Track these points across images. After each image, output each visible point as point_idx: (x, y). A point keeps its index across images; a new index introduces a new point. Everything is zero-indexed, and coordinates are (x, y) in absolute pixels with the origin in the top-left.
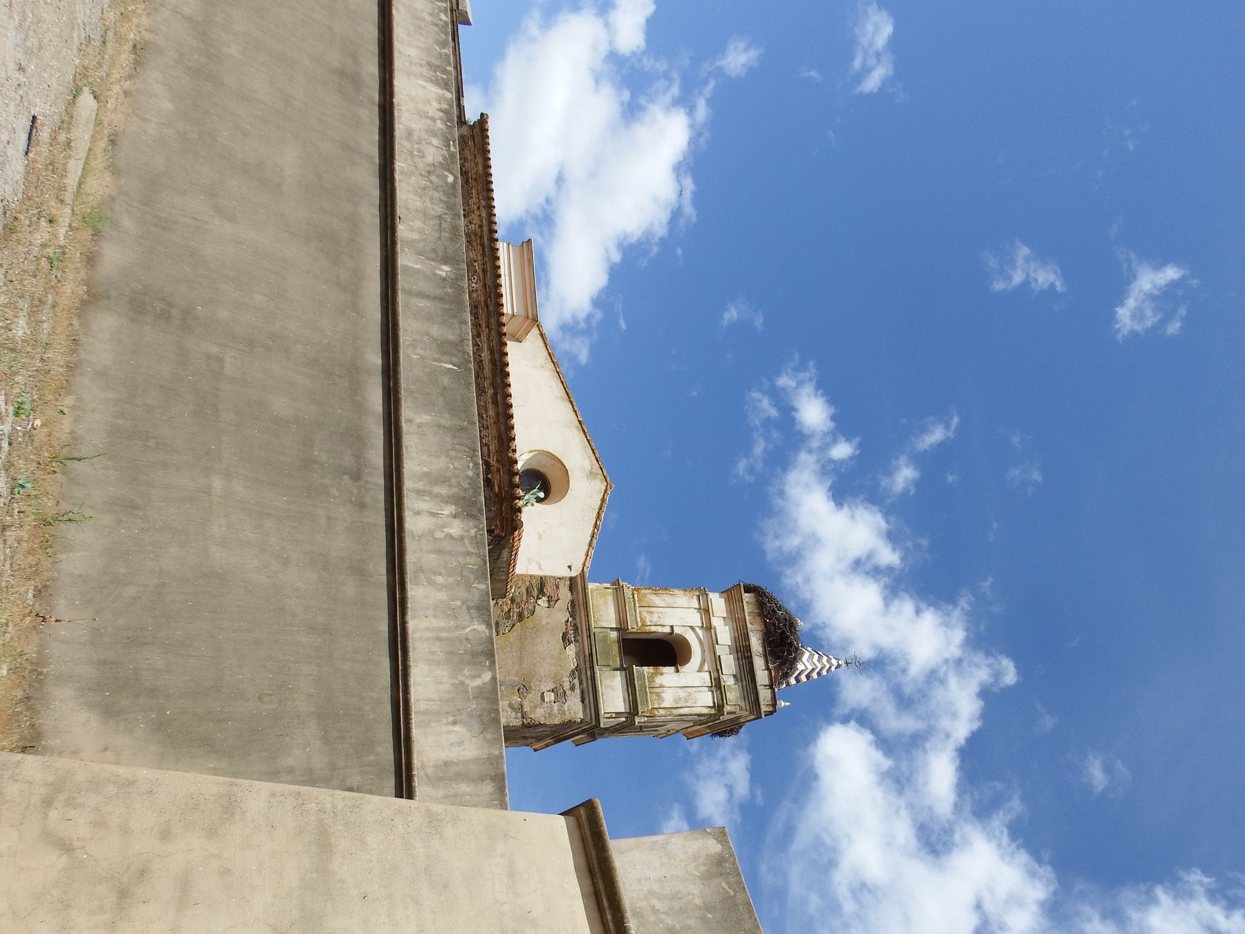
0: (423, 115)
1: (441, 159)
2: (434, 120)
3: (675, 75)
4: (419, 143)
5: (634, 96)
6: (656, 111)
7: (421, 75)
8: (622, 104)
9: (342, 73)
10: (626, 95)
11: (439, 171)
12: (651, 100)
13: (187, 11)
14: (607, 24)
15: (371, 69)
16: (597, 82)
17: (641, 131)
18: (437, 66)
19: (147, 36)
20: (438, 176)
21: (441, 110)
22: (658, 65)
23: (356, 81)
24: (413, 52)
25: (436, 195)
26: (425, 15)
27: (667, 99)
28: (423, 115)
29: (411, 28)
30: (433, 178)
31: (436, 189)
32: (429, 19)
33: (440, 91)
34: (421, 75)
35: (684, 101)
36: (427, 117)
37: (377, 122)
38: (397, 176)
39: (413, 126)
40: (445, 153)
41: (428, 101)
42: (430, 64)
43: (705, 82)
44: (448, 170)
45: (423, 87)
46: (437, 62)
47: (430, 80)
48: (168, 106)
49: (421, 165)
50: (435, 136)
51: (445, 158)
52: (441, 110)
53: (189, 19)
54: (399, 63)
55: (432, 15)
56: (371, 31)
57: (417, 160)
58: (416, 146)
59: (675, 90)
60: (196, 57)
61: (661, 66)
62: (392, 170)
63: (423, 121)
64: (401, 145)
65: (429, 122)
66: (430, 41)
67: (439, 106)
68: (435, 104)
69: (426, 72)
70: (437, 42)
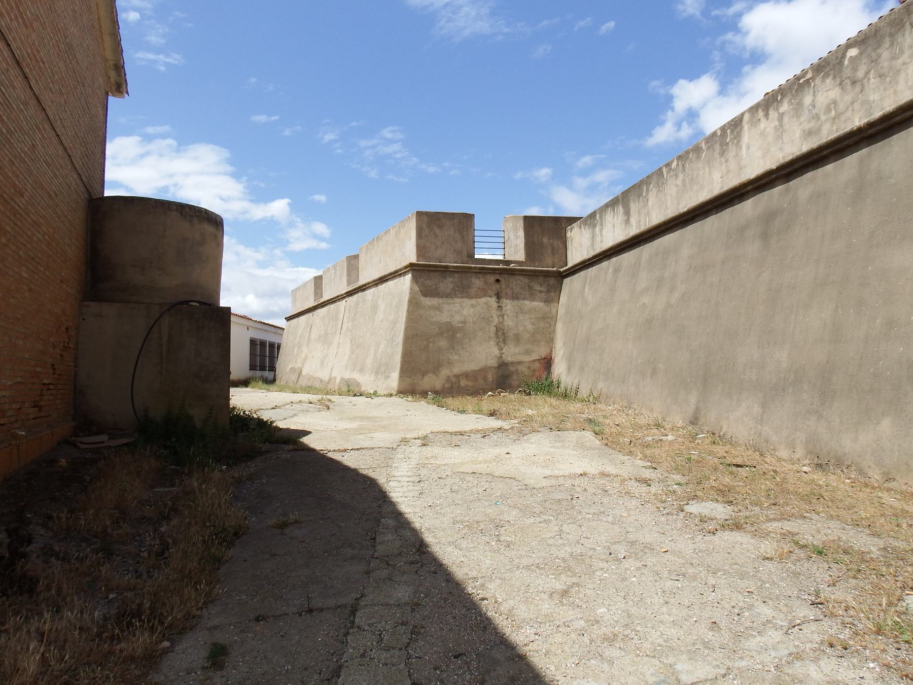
0: (780, 129)
1: (829, 81)
2: (782, 115)
3: (718, 42)
4: (817, 117)
5: (746, 63)
6: (750, 41)
7: (737, 155)
8: (754, 68)
9: (765, 236)
10: (746, 69)
11: (847, 72)
12: (744, 48)
13: (757, 409)
14: (704, 105)
15: (748, 207)
16: (745, 94)
17: (771, 44)
18: (721, 145)
19: (800, 452)
20: (855, 70)
21: (767, 115)
22: (717, 59)
23: (769, 217)
24: (716, 176)
25: (886, 55)
26: (679, 182)
27: (738, 39)
28: (780, 129)
29: (695, 188)
30: (860, 74)
31: (875, 61)
32: (681, 176)
33: (746, 127)
34: (737, 155)
35: (733, 25)
36: (781, 125)
37: (809, 175)
38: (877, 114)
39: (798, 134)
40: (818, 81)
41: (763, 134)
42: (722, 153)
43: (717, 18)
44: (841, 63)
45: (748, 147)
46: (717, 147)
47: (738, 145)
48: (886, 425)
49: (848, 98)
50: (800, 104)
51: (827, 75)
52: (767, 115)
53: (764, 405)
54: (733, 181)
55: (677, 176)
56: (712, 223)
57: (841, 106)
58: (823, 118)
59: (729, 36)
60: (805, 396)
61: (716, 55)
62: (871, 125)
63: (786, 126)
64: (828, 133)
65: (786, 119)
66: (700, 165)
67: (763, 120)
68: (763, 124)
69: (731, 152)
70: (698, 157)
